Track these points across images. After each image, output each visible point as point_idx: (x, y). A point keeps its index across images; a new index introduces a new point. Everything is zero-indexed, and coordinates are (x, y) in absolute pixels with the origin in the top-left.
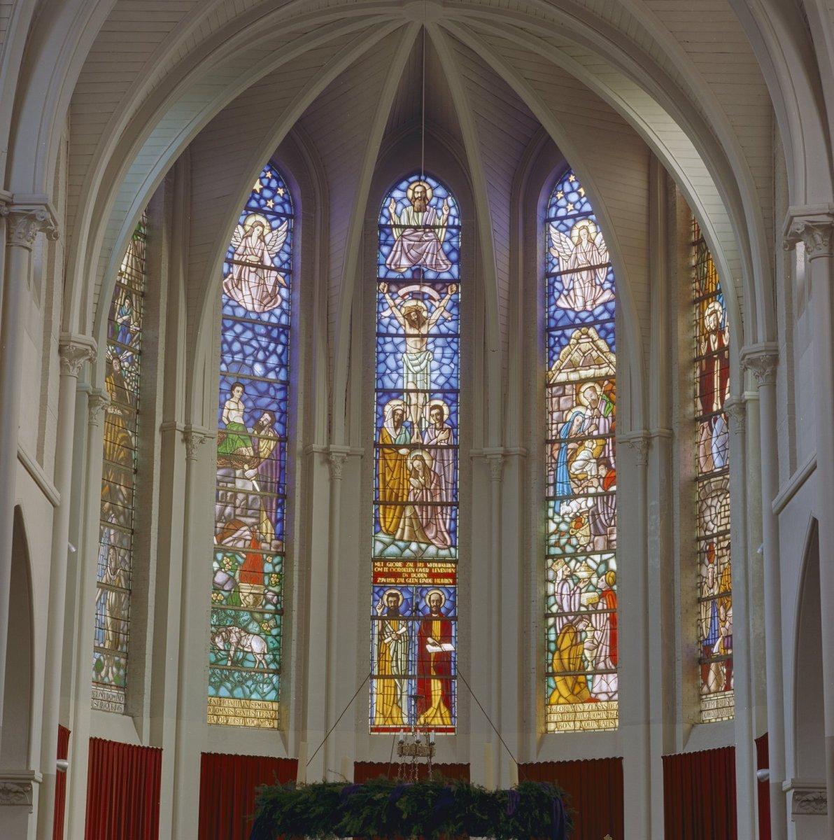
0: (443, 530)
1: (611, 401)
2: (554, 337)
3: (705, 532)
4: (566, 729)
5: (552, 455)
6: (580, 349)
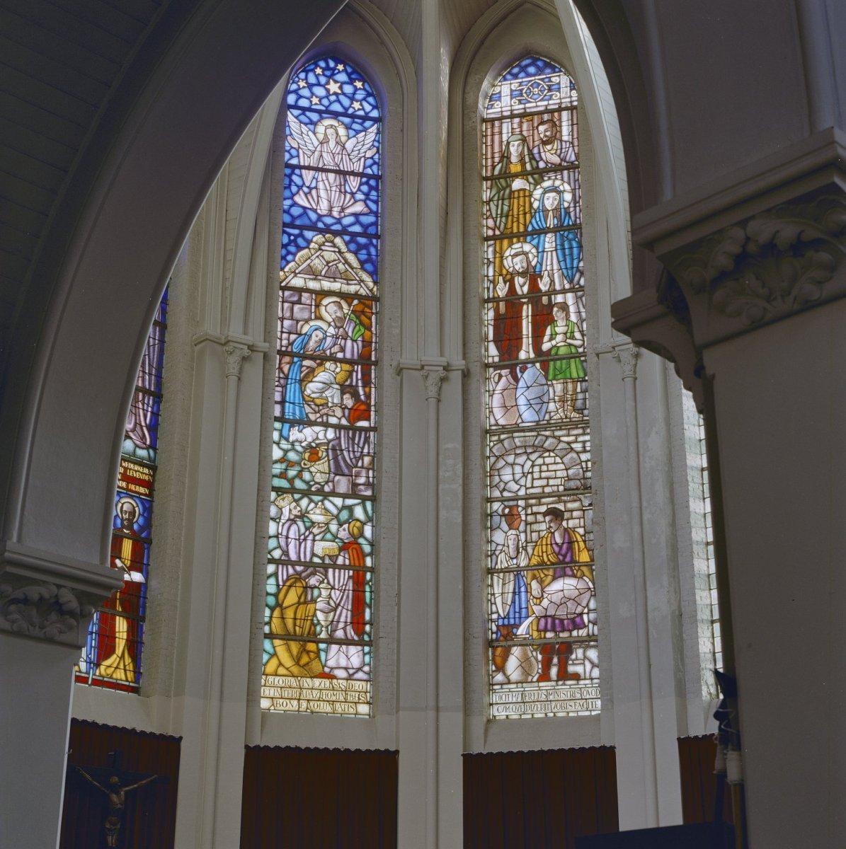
0: (143, 424)
1: (361, 323)
2: (290, 235)
3: (501, 492)
4: (287, 708)
5: (280, 369)
6: (323, 257)
